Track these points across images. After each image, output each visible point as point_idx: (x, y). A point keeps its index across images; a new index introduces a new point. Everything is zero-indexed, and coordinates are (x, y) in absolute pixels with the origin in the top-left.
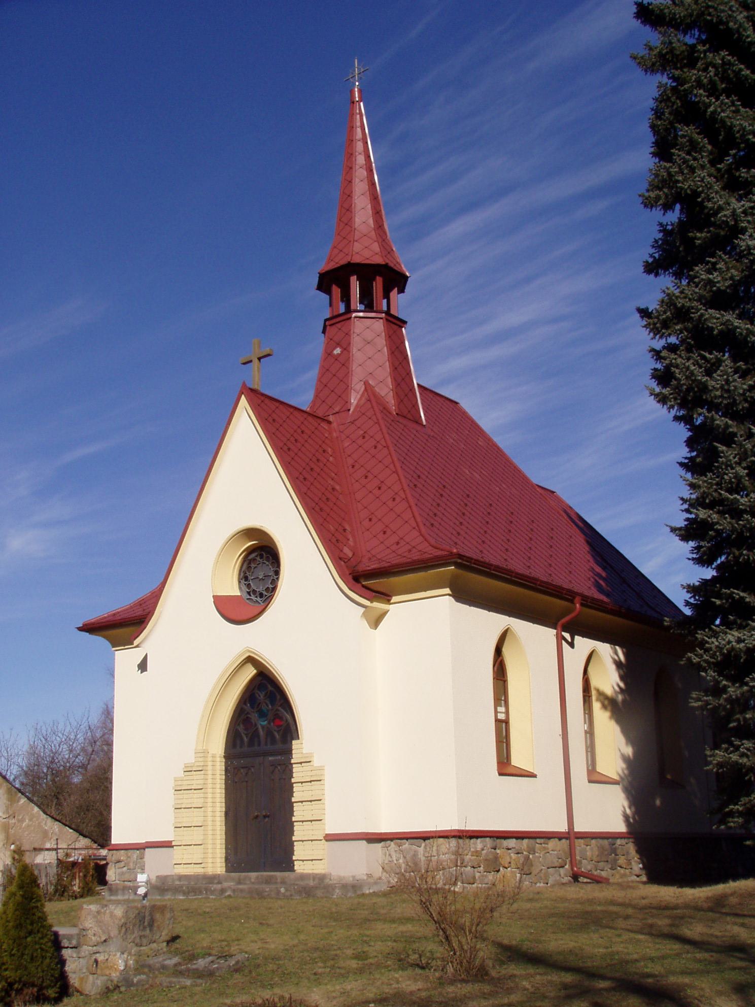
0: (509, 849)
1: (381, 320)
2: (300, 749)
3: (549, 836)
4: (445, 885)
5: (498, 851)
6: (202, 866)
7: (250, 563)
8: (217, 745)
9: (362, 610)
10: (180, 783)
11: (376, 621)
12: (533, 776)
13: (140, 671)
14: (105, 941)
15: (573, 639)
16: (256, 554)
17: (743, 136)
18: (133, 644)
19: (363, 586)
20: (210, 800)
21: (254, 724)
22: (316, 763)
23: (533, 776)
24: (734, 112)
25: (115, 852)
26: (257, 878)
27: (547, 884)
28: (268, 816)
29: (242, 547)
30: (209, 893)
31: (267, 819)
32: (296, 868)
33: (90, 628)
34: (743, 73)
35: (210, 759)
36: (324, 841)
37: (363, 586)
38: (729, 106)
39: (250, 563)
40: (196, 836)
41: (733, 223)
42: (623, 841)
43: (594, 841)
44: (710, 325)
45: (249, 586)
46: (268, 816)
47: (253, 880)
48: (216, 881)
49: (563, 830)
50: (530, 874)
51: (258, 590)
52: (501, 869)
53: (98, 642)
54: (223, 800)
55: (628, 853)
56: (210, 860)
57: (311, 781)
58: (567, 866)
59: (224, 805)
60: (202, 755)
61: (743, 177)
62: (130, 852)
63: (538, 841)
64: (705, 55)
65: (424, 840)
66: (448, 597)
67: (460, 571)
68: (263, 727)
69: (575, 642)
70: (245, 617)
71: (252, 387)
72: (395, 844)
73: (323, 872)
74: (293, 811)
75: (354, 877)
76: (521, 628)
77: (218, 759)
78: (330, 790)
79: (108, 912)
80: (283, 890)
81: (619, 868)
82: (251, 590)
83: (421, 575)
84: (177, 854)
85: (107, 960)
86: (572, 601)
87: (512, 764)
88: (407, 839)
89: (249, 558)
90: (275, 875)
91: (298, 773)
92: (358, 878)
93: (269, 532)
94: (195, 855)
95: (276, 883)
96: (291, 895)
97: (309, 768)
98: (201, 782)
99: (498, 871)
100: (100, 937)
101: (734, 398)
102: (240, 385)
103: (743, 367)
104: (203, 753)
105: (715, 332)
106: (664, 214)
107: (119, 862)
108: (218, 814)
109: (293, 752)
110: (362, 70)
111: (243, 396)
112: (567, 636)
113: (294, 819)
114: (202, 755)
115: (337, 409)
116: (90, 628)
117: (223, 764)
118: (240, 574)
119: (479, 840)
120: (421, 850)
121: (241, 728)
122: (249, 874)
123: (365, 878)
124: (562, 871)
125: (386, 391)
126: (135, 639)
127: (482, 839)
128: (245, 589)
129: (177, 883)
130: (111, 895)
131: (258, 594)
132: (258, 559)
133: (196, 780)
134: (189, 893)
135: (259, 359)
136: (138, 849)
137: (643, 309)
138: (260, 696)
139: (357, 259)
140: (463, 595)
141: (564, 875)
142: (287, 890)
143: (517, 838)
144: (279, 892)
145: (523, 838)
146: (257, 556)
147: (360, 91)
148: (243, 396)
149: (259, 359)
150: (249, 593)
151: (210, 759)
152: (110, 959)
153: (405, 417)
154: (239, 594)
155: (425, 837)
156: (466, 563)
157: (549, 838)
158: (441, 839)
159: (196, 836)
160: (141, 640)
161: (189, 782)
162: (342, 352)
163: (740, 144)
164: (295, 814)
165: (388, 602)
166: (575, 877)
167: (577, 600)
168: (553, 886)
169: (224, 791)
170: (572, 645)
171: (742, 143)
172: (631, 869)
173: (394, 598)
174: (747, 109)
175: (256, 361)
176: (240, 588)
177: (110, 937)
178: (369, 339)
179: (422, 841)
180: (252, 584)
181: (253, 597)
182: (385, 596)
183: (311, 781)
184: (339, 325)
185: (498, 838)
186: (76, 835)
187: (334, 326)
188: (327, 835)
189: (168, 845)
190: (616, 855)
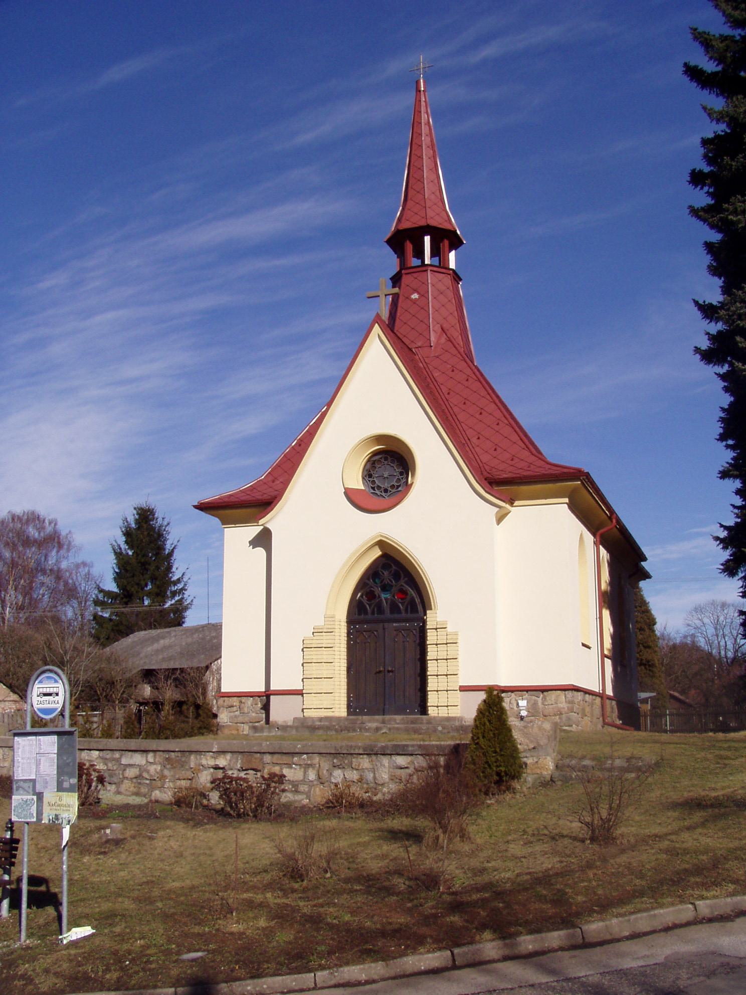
6: (332, 710)
13: (251, 547)
14: (534, 748)
16: (380, 456)
18: (258, 523)
21: (377, 596)
22: (450, 629)
25: (226, 698)
26: (403, 719)
29: (369, 450)
30: (363, 731)
31: (391, 674)
32: (429, 713)
33: (203, 507)
45: (373, 482)
47: (398, 721)
51: (382, 486)
53: (210, 521)
62: (244, 699)
65: (543, 692)
67: (581, 486)
68: (386, 599)
70: (369, 507)
72: (516, 695)
78: (462, 651)
79: (535, 726)
82: (376, 485)
83: (550, 486)
85: (537, 762)
88: (527, 691)
89: (372, 459)
90: (421, 718)
94: (325, 701)
95: (421, 723)
100: (528, 745)
104: (330, 618)
116: (203, 507)
120: (540, 700)
122: (395, 716)
129: (318, 723)
130: (256, 732)
131: (382, 489)
132: (383, 460)
136: (251, 697)
137: (393, 283)
138: (383, 574)
139: (433, 223)
146: (381, 458)
149: (386, 295)
150: (373, 488)
152: (539, 762)
155: (544, 690)
158: (559, 692)
160: (269, 518)
161: (318, 642)
177: (539, 745)
180: (376, 481)
181: (377, 492)
184: (415, 275)
186: (7, 691)
187: (410, 275)
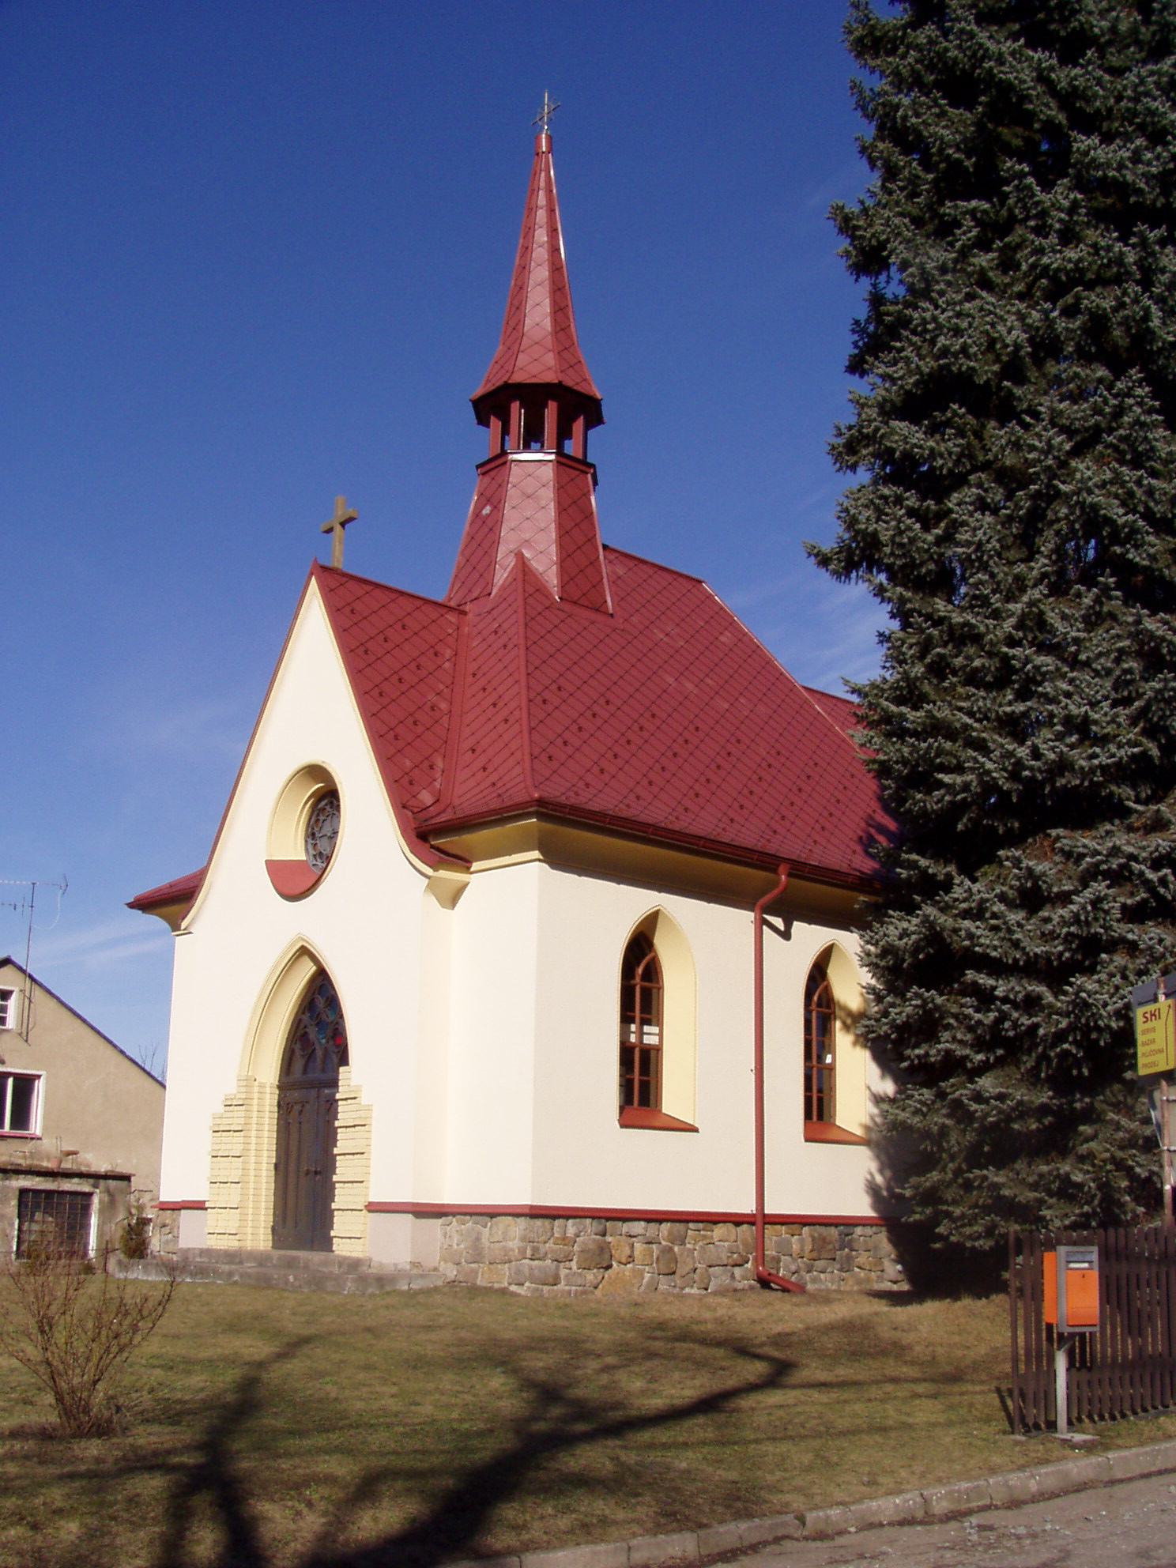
0: (630, 1236)
1: (550, 464)
2: (349, 1078)
3: (714, 1218)
4: (510, 1284)
5: (609, 1239)
6: (237, 1237)
7: (318, 815)
8: (269, 1070)
9: (427, 881)
10: (218, 1121)
11: (452, 898)
12: (693, 1129)
15: (788, 926)
17: (941, 150)
19: (432, 847)
20: (253, 1147)
22: (364, 1099)
23: (693, 1129)
24: (938, 116)
27: (706, 1289)
28: (320, 1173)
34: (949, 54)
35: (256, 1089)
36: (365, 1212)
37: (432, 847)
38: (931, 107)
39: (318, 815)
40: (232, 1196)
41: (923, 286)
42: (869, 1230)
43: (806, 1230)
44: (888, 444)
46: (320, 1173)
48: (237, 1260)
49: (748, 1211)
50: (674, 1273)
52: (615, 1264)
53: (153, 922)
54: (274, 1147)
55: (876, 1248)
56: (250, 1231)
57: (354, 1126)
58: (749, 1265)
59: (274, 1154)
60: (244, 1083)
61: (949, 215)
63: (691, 1225)
64: (905, 34)
66: (537, 863)
67: (549, 826)
69: (793, 931)
70: (298, 891)
71: (326, 564)
73: (360, 1255)
74: (335, 1168)
75: (395, 1265)
76: (679, 909)
77: (268, 1090)
80: (291, 1278)
81: (856, 1269)
84: (211, 1220)
86: (775, 871)
87: (664, 1111)
88: (471, 1214)
91: (345, 1114)
92: (399, 1267)
93: (330, 770)
94: (224, 1221)
96: (300, 1287)
97: (354, 1107)
98: (242, 1121)
99: (609, 1267)
101: (912, 557)
102: (311, 563)
103: (933, 507)
104: (248, 1081)
105: (897, 454)
106: (856, 280)
107: (164, 1226)
108: (264, 1166)
109: (340, 1083)
110: (553, 107)
111: (313, 578)
112: (778, 922)
113: (335, 1178)
114: (244, 1083)
115: (475, 595)
117: (276, 1097)
118: (307, 830)
119: (571, 1221)
121: (298, 1047)
123: (408, 1267)
124: (737, 1271)
125: (546, 564)
126: (183, 919)
127: (578, 1220)
128: (312, 852)
132: (328, 808)
133: (237, 1119)
134: (196, 1274)
135: (343, 524)
139: (518, 378)
140: (560, 858)
141: (743, 1276)
142: (295, 1279)
143: (648, 1221)
144: (287, 1282)
145: (660, 1221)
147: (550, 139)
148: (313, 578)
149: (343, 524)
151: (256, 1089)
153: (575, 603)
154: (304, 858)
155: (491, 1213)
156: (548, 810)
157: (716, 1223)
159: (232, 1196)
162: (492, 511)
163: (938, 163)
164: (338, 1171)
165: (467, 869)
166: (765, 1283)
167: (782, 868)
168: (715, 1293)
169: (275, 1135)
170: (786, 935)
171: (941, 162)
172: (882, 1271)
173: (474, 864)
174: (961, 110)
175: (338, 529)
176: (307, 850)
178: (530, 491)
179: (488, 1219)
182: (462, 861)
183: (354, 1126)
184: (492, 473)
185: (608, 1219)
188: (370, 1204)
189: (199, 1206)
190: (852, 1250)
